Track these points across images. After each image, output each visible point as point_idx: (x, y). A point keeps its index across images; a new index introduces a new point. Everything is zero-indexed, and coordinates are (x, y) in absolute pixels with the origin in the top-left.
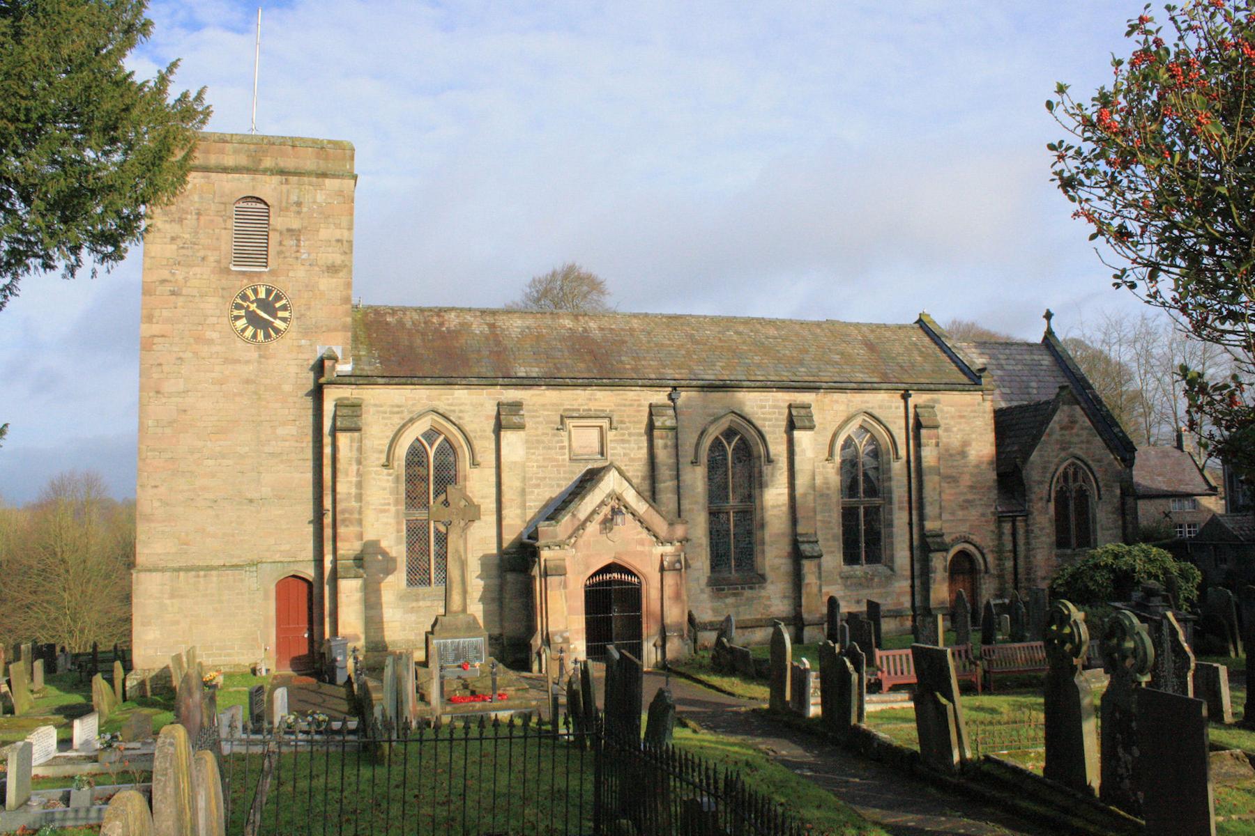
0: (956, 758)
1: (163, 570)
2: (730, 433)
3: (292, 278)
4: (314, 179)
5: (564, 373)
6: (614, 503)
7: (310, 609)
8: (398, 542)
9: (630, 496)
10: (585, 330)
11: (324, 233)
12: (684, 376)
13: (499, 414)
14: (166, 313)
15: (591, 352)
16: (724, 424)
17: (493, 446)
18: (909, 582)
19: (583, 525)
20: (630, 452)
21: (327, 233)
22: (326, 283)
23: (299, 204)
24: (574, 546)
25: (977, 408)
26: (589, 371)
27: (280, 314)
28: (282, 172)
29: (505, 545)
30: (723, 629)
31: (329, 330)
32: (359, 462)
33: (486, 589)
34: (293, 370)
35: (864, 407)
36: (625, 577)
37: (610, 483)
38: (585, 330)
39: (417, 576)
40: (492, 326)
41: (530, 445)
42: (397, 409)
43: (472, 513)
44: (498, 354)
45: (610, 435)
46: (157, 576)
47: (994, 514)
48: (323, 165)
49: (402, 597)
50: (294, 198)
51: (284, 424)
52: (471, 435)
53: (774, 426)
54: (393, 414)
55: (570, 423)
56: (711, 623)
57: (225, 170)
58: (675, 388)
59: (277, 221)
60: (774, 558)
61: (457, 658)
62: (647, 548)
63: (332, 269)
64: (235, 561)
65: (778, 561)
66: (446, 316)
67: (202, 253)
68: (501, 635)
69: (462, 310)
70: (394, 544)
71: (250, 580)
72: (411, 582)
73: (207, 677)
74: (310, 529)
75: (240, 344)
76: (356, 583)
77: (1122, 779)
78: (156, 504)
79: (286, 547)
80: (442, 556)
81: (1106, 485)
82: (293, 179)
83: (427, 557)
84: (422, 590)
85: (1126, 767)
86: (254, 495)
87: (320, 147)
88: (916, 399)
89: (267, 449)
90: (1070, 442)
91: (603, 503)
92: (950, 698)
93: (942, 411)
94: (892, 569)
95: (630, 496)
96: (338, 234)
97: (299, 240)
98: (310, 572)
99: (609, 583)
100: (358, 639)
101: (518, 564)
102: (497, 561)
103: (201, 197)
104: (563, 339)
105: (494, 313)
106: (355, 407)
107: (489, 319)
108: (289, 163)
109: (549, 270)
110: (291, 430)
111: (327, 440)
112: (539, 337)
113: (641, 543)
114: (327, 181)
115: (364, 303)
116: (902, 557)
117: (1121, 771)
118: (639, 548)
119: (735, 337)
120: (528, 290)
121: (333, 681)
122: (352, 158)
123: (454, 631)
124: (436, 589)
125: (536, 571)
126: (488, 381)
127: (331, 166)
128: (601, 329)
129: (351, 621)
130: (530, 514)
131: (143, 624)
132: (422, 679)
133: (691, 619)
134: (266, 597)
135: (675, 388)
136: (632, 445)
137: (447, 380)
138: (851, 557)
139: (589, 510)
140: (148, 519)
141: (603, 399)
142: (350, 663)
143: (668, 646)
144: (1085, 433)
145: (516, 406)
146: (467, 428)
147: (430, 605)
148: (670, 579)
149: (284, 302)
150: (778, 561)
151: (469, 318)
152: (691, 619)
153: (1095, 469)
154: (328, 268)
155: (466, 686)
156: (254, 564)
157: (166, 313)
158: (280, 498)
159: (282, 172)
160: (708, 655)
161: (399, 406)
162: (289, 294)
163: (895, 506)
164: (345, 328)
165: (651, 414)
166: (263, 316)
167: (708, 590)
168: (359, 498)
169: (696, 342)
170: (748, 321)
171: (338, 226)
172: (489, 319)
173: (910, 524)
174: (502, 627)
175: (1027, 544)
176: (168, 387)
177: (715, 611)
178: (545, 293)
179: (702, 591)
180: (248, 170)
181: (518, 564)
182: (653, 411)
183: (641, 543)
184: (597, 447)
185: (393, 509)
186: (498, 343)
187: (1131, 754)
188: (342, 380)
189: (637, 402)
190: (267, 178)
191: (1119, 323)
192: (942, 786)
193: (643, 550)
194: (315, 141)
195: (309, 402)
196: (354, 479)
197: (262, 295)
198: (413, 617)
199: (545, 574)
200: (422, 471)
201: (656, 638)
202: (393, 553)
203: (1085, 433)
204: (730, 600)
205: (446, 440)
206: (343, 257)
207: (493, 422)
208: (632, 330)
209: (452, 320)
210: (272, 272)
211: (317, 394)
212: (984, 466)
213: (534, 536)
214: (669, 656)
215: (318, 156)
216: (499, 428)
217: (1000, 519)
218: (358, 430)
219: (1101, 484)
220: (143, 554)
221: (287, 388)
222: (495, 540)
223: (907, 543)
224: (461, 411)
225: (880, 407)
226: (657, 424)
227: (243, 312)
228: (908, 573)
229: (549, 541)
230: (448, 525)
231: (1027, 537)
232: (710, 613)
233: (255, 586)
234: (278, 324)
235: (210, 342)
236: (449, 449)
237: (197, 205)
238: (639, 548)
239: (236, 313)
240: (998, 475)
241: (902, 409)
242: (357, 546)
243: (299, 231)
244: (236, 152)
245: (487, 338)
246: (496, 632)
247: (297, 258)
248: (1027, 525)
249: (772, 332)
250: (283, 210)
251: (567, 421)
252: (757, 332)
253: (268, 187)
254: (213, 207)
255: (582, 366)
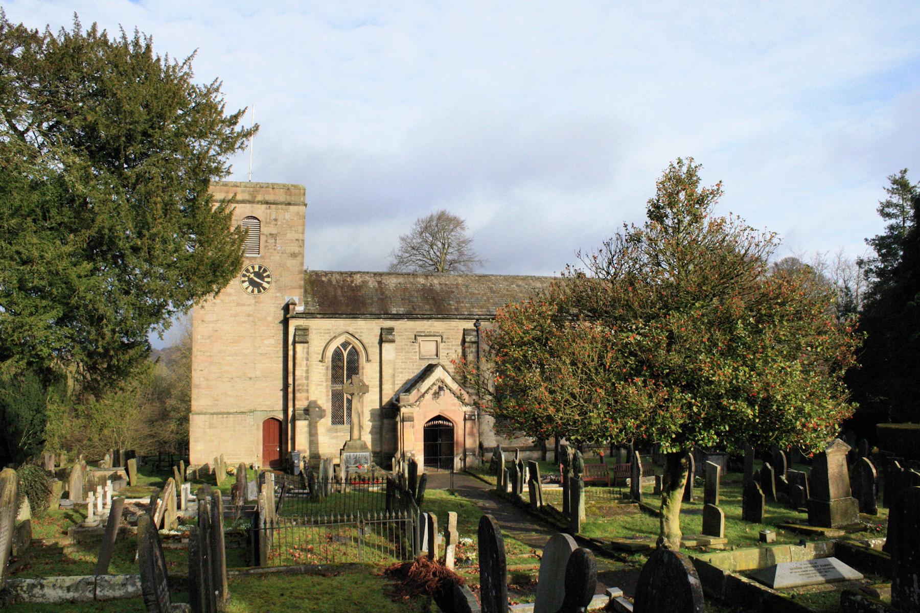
0: (538, 504)
1: (205, 414)
4: (284, 206)
5: (417, 311)
6: (440, 384)
7: (280, 435)
8: (327, 402)
9: (449, 381)
10: (431, 285)
13: (381, 334)
15: (433, 299)
17: (378, 351)
19: (423, 396)
20: (451, 351)
21: (291, 235)
22: (291, 263)
26: (431, 310)
27: (266, 279)
29: (383, 404)
30: (496, 451)
32: (307, 360)
33: (373, 427)
34: (273, 309)
36: (446, 423)
37: (438, 373)
38: (431, 285)
39: (337, 419)
40: (380, 283)
41: (398, 351)
43: (364, 389)
44: (382, 300)
45: (441, 346)
48: (289, 199)
49: (329, 430)
50: (273, 217)
51: (267, 338)
52: (366, 345)
54: (326, 333)
58: (477, 320)
61: (355, 463)
62: (456, 408)
63: (294, 255)
64: (242, 410)
66: (355, 277)
68: (381, 452)
69: (364, 273)
70: (325, 403)
71: (250, 420)
72: (333, 423)
73: (229, 469)
74: (281, 393)
75: (245, 296)
76: (306, 422)
78: (202, 379)
79: (268, 403)
80: (350, 409)
82: (273, 206)
83: (341, 412)
84: (339, 427)
86: (253, 376)
87: (287, 189)
89: (260, 351)
91: (434, 384)
92: (537, 481)
95: (449, 381)
96: (296, 236)
98: (280, 416)
99: (439, 425)
100: (305, 452)
101: (389, 414)
102: (379, 412)
104: (418, 291)
105: (381, 275)
106: (306, 330)
107: (379, 279)
108: (270, 198)
110: (272, 341)
111: (291, 347)
112: (406, 289)
113: (454, 405)
114: (291, 207)
115: (311, 269)
119: (516, 288)
120: (414, 227)
121: (292, 473)
122: (304, 194)
123: (354, 449)
124: (346, 426)
125: (398, 419)
126: (376, 316)
127: (293, 199)
128: (440, 284)
129: (302, 443)
130: (397, 387)
131: (195, 441)
132: (338, 472)
133: (481, 445)
134: (258, 429)
135: (477, 320)
137: (354, 315)
140: (198, 387)
141: (438, 326)
142: (302, 464)
143: (467, 459)
145: (391, 330)
146: (364, 342)
147: (343, 434)
148: (469, 424)
151: (367, 278)
152: (481, 445)
155: (359, 477)
156: (252, 412)
158: (265, 377)
159: (267, 203)
160: (488, 465)
162: (271, 269)
164: (300, 287)
165: (464, 335)
168: (307, 378)
169: (493, 292)
170: (525, 278)
171: (297, 232)
172: (379, 279)
174: (381, 447)
178: (426, 229)
180: (249, 202)
181: (389, 414)
182: (466, 332)
183: (454, 405)
184: (435, 353)
185: (325, 384)
186: (383, 293)
188: (298, 316)
189: (456, 328)
190: (259, 206)
192: (533, 515)
193: (455, 409)
194: (284, 185)
195: (281, 327)
196: (305, 369)
197: (257, 269)
198: (334, 441)
199: (403, 420)
200: (340, 364)
201: (461, 455)
202: (324, 407)
205: (353, 347)
207: (378, 338)
208: (458, 284)
209: (358, 280)
210: (262, 257)
211: (285, 323)
213: (398, 400)
214: (467, 464)
216: (381, 342)
218: (307, 342)
220: (196, 405)
221: (270, 319)
222: (378, 401)
226: (467, 340)
227: (246, 279)
229: (405, 403)
230: (352, 395)
233: (252, 423)
234: (265, 285)
236: (354, 353)
239: (243, 279)
242: (306, 403)
245: (376, 290)
246: (378, 450)
251: (418, 338)
252: (530, 284)
255: (427, 307)
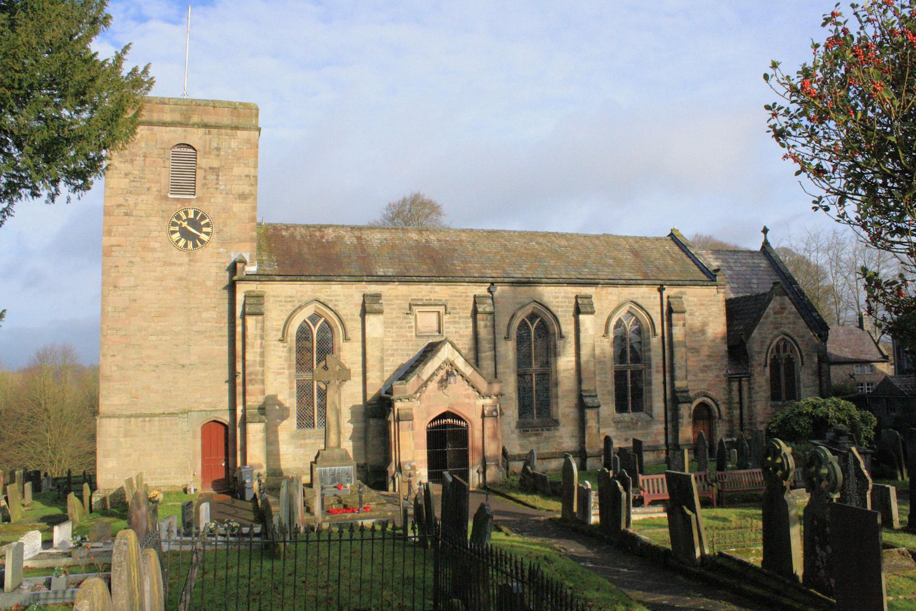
0: (698, 554)
1: (119, 417)
2: (533, 317)
3: (213, 203)
4: (229, 131)
5: (412, 273)
6: (448, 368)
7: (226, 445)
8: (291, 396)
9: (460, 363)
10: (427, 241)
11: (237, 171)
12: (499, 275)
13: (364, 302)
14: (121, 229)
15: (432, 257)
16: (528, 310)
17: (360, 326)
18: (663, 425)
19: (425, 384)
20: (460, 330)
21: (238, 170)
22: (238, 207)
23: (218, 149)
24: (419, 399)
25: (713, 298)
26: (430, 271)
27: (205, 229)
28: (206, 126)
29: (369, 398)
30: (528, 460)
31: (240, 241)
32: (262, 338)
33: (355, 430)
34: (214, 270)
35: (631, 297)
36: (456, 422)
37: (446, 353)
38: (427, 241)
39: (305, 421)
40: (359, 238)
41: (387, 325)
42: (290, 299)
43: (344, 375)
44: (364, 258)
45: (446, 318)
46: (115, 421)
47: (725, 375)
48: (236, 121)
49: (294, 436)
50: (214, 145)
51: (207, 310)
52: (344, 318)
53: (565, 311)
54: (287, 303)
55: (416, 309)
56: (519, 456)
57: (164, 124)
58: (492, 284)
59: (202, 162)
60: (565, 407)
61: (333, 481)
62: (472, 401)
63: (243, 197)
64: (171, 410)
65: (568, 410)
66: (326, 231)
67: (147, 185)
68: (366, 464)
69: (337, 226)
70: (288, 398)
71: (183, 424)
72: (300, 426)
73: (151, 495)
74: (226, 387)
75: (175, 251)
76: (260, 426)
77: (819, 569)
78: (114, 368)
79: (209, 400)
80: (323, 406)
81: (807, 355)
82: (214, 131)
83: (312, 407)
84: (308, 431)
85: (822, 561)
86: (186, 362)
87: (234, 108)
88: (669, 291)
89: (195, 328)
90: (781, 323)
91: (440, 368)
92: (694, 510)
93: (687, 300)
94: (651, 416)
95: (460, 363)
96: (247, 171)
97: (218, 176)
98: (226, 418)
99: (445, 426)
100: (261, 467)
101: (378, 412)
102: (363, 410)
103: (147, 144)
104: (411, 248)
105: (360, 229)
106: (259, 298)
107: (357, 233)
108: (211, 119)
109: (400, 198)
110: (213, 314)
111: (239, 322)
112: (393, 247)
113: (468, 397)
114: (239, 132)
115: (266, 221)
116: (658, 407)
117: (818, 563)
118: (466, 401)
119: (537, 246)
120: (385, 212)
121: (243, 498)
122: (257, 115)
123: (331, 461)
124: (319, 430)
125: (391, 417)
126: (356, 279)
127: (242, 121)
128: (439, 241)
129: (256, 454)
130: (387, 376)
131: (105, 456)
132: (308, 496)
133: (504, 453)
134: (194, 436)
135: (492, 284)
136: (462, 325)
137: (327, 278)
138: (621, 407)
139: (430, 373)
140: (108, 379)
141: (440, 291)
142: (256, 485)
143: (488, 472)
144: (792, 316)
145: (377, 297)
146: (341, 313)
147: (314, 442)
148: (489, 423)
149: (207, 221)
150: (568, 410)
151: (342, 232)
152: (504, 453)
153: (799, 342)
154: (240, 196)
155: (340, 502)
156: (186, 412)
157: (121, 229)
158: (204, 364)
159: (206, 126)
160: (517, 479)
161: (291, 297)
162: (211, 215)
163: (654, 370)
164: (251, 240)
165: (475, 303)
166: (192, 231)
167: (517, 431)
168: (262, 364)
169: (508, 250)
170: (546, 235)
171: (247, 165)
172: (357, 233)
173: (664, 383)
174: (366, 458)
175: (750, 397)
176: (122, 283)
177: (522, 446)
178: (398, 214)
179: (513, 432)
180: (181, 124)
181: (378, 412)
182: (476, 300)
183: (468, 397)
184: (435, 327)
185: (287, 372)
186: (363, 251)
187: (825, 551)
188: (249, 278)
189: (465, 294)
190: (195, 130)
191: (817, 236)
192: (688, 574)
193: (469, 402)
194: (230, 103)
195: (226, 294)
196: (259, 350)
197: (191, 216)
198: (301, 451)
199: (398, 420)
200: (308, 344)
201: (479, 466)
202: (287, 404)
203: (792, 316)
204: (533, 439)
205: (326, 321)
206: (250, 188)
207: (359, 308)
208: (461, 241)
209: (330, 234)
210: (199, 199)
211: (232, 288)
212: (718, 341)
213: (390, 392)
214: (488, 479)
215: (232, 114)
216: (364, 313)
217: (730, 379)
218: (261, 314)
219: (803, 354)
220: (105, 405)
221: (209, 283)
222: (361, 395)
223: (662, 397)
224: (336, 301)
225: (642, 298)
226: (480, 310)
227: (177, 228)
228: (663, 419)
229: (401, 395)
230: (327, 383)
231: (750, 393)
232: (518, 448)
233: (186, 428)
234: (203, 237)
235: (153, 250)
236: (327, 328)
237: (144, 150)
238: (466, 401)
239: (172, 229)
240: (729, 347)
241: (659, 299)
242: (260, 399)
243: (219, 169)
244: (172, 111)
245: (355, 247)
246: (362, 462)
247: (217, 189)
248: (750, 384)
249: (564, 242)
250: (207, 153)
251: (414, 308)
252: (552, 242)
253: (195, 137)
254: (156, 151)
255: (425, 267)
